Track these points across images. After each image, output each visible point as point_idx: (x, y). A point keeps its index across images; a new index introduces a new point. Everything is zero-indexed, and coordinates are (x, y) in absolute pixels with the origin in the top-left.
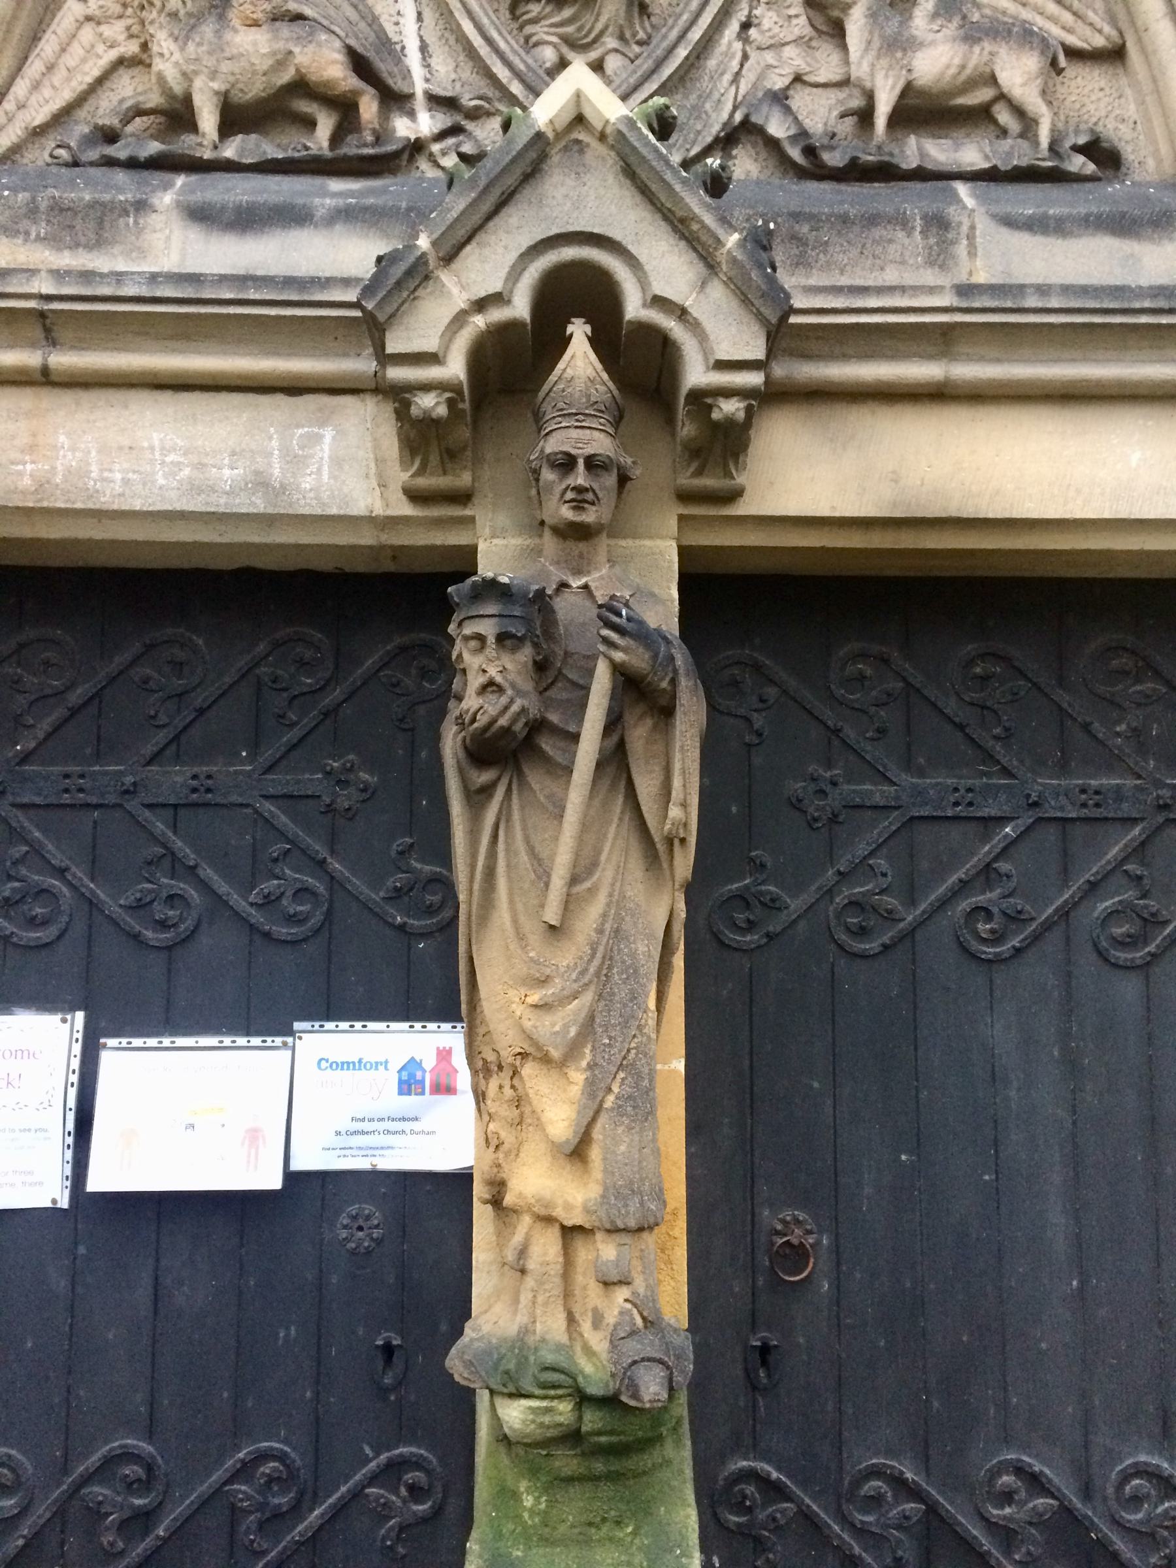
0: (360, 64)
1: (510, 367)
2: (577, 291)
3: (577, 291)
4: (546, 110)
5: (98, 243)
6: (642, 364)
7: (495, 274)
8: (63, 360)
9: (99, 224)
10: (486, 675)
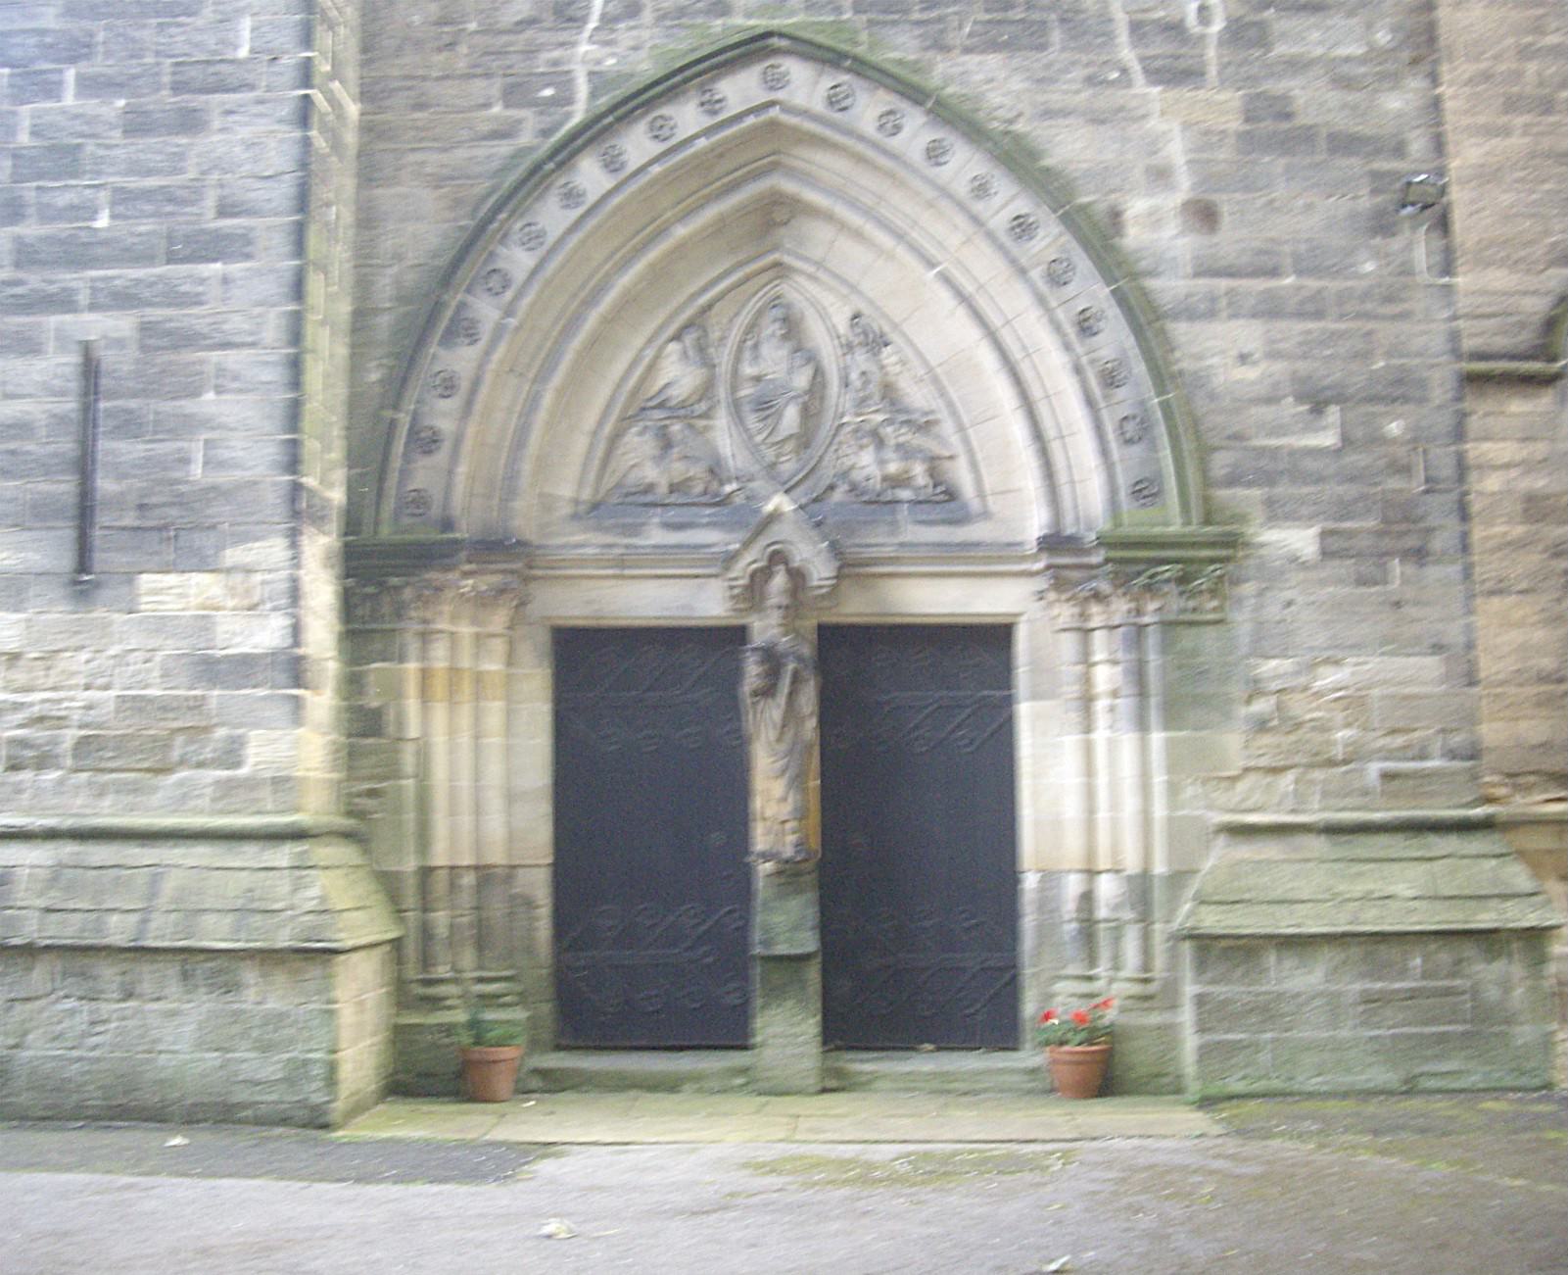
0: (711, 471)
1: (759, 579)
2: (777, 558)
3: (777, 558)
4: (769, 507)
5: (636, 535)
6: (797, 577)
7: (751, 559)
8: (627, 572)
9: (634, 530)
10: (753, 671)
